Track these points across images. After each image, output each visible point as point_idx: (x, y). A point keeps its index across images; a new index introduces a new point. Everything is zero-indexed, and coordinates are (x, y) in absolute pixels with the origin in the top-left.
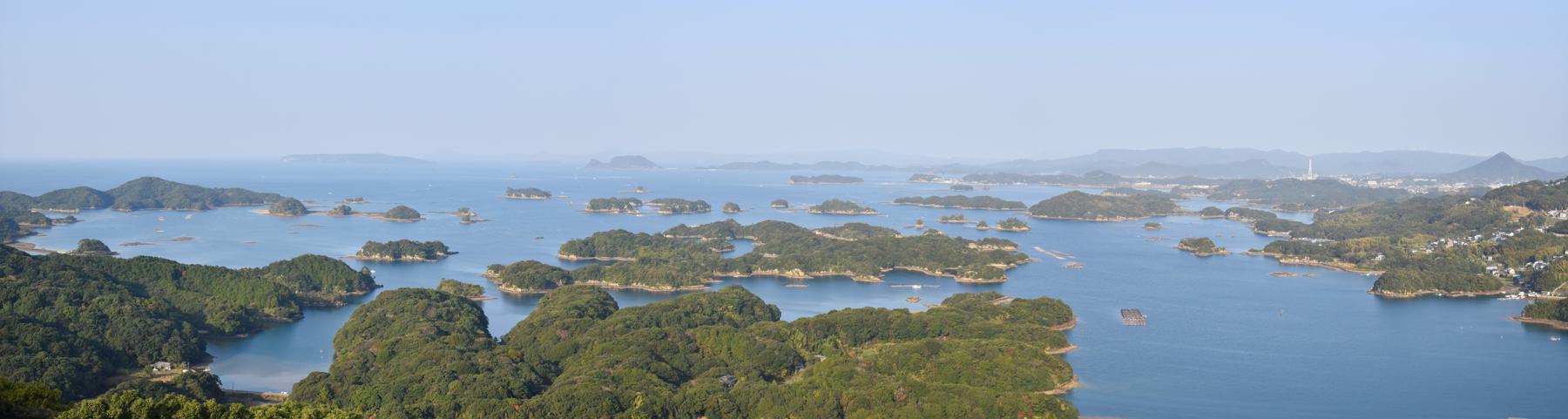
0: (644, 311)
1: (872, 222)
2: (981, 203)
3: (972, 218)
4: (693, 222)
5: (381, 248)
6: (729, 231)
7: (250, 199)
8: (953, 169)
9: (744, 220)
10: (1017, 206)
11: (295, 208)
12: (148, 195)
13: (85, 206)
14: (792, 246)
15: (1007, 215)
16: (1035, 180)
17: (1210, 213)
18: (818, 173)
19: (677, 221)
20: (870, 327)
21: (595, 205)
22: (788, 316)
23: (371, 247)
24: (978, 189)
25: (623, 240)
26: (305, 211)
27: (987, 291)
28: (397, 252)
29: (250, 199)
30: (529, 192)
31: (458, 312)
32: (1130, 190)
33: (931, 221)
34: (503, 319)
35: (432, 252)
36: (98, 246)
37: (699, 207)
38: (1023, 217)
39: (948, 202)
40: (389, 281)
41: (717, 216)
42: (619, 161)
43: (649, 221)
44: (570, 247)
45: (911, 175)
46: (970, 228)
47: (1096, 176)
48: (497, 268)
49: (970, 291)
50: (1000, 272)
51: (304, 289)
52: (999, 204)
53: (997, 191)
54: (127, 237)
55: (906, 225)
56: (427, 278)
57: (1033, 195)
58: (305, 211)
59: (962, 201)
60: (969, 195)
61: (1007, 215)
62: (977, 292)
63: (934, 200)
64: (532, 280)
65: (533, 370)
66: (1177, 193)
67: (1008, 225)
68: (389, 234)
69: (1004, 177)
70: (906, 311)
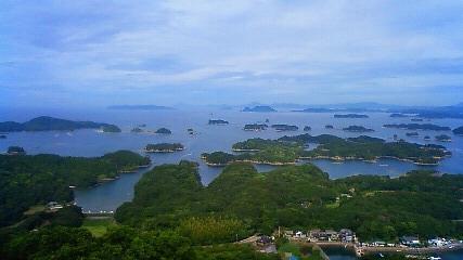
0: (270, 173)
1: (372, 135)
3: (422, 133)
4: (290, 134)
5: (155, 147)
6: (306, 139)
7: (97, 126)
10: (447, 129)
11: (114, 129)
12: (45, 123)
13: (11, 130)
14: (330, 145)
15: (442, 133)
19: (283, 134)
20: (374, 183)
21: (248, 127)
22: (333, 178)
23: (149, 147)
24: (425, 121)
25: (258, 143)
26: (158, 132)
27: (430, 169)
28: (162, 148)
29: (97, 126)
30: (218, 122)
31: (187, 170)
33: (402, 135)
35: (176, 147)
36: (20, 150)
37: (294, 128)
39: (411, 127)
40: (157, 161)
42: (110, 108)
43: (272, 135)
44: (236, 146)
46: (420, 139)
48: (205, 155)
49: (421, 168)
50: (436, 161)
51: (121, 162)
52: (437, 128)
53: (434, 122)
54: (33, 144)
55: (388, 137)
56: (173, 159)
58: (119, 130)
59: (417, 127)
61: (442, 133)
62: (425, 169)
63: (402, 126)
64: (216, 159)
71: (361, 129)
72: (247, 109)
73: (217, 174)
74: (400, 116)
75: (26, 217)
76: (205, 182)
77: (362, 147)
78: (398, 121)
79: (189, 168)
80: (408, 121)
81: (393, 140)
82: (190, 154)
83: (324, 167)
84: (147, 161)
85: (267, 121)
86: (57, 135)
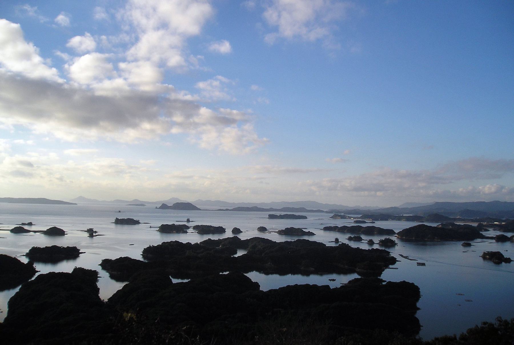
1: (312, 239)
2: (371, 231)
4: (215, 237)
6: (235, 243)
8: (355, 211)
9: (243, 237)
10: (390, 232)
16: (399, 218)
17: (501, 239)
18: (283, 213)
19: (206, 238)
32: (453, 225)
34: (108, 288)
35: (72, 253)
37: (221, 230)
38: (394, 238)
40: (43, 269)
41: (229, 234)
45: (332, 215)
47: (435, 217)
52: (381, 232)
53: (379, 224)
56: (66, 267)
57: (398, 226)
60: (364, 225)
64: (117, 267)
65: (164, 25)
66: (481, 227)
67: (383, 243)
68: (44, 242)
69: (385, 216)
70: (328, 287)
71: (299, 232)
72: (164, 206)
73: (119, 286)
74: (343, 217)
75: (198, 91)
76: (125, 314)
77: (297, 254)
78: (340, 223)
79: (90, 277)
80: (350, 223)
81: (333, 245)
82: (89, 260)
83: (254, 276)
84: (29, 269)
85: (188, 221)
86: (461, 190)
